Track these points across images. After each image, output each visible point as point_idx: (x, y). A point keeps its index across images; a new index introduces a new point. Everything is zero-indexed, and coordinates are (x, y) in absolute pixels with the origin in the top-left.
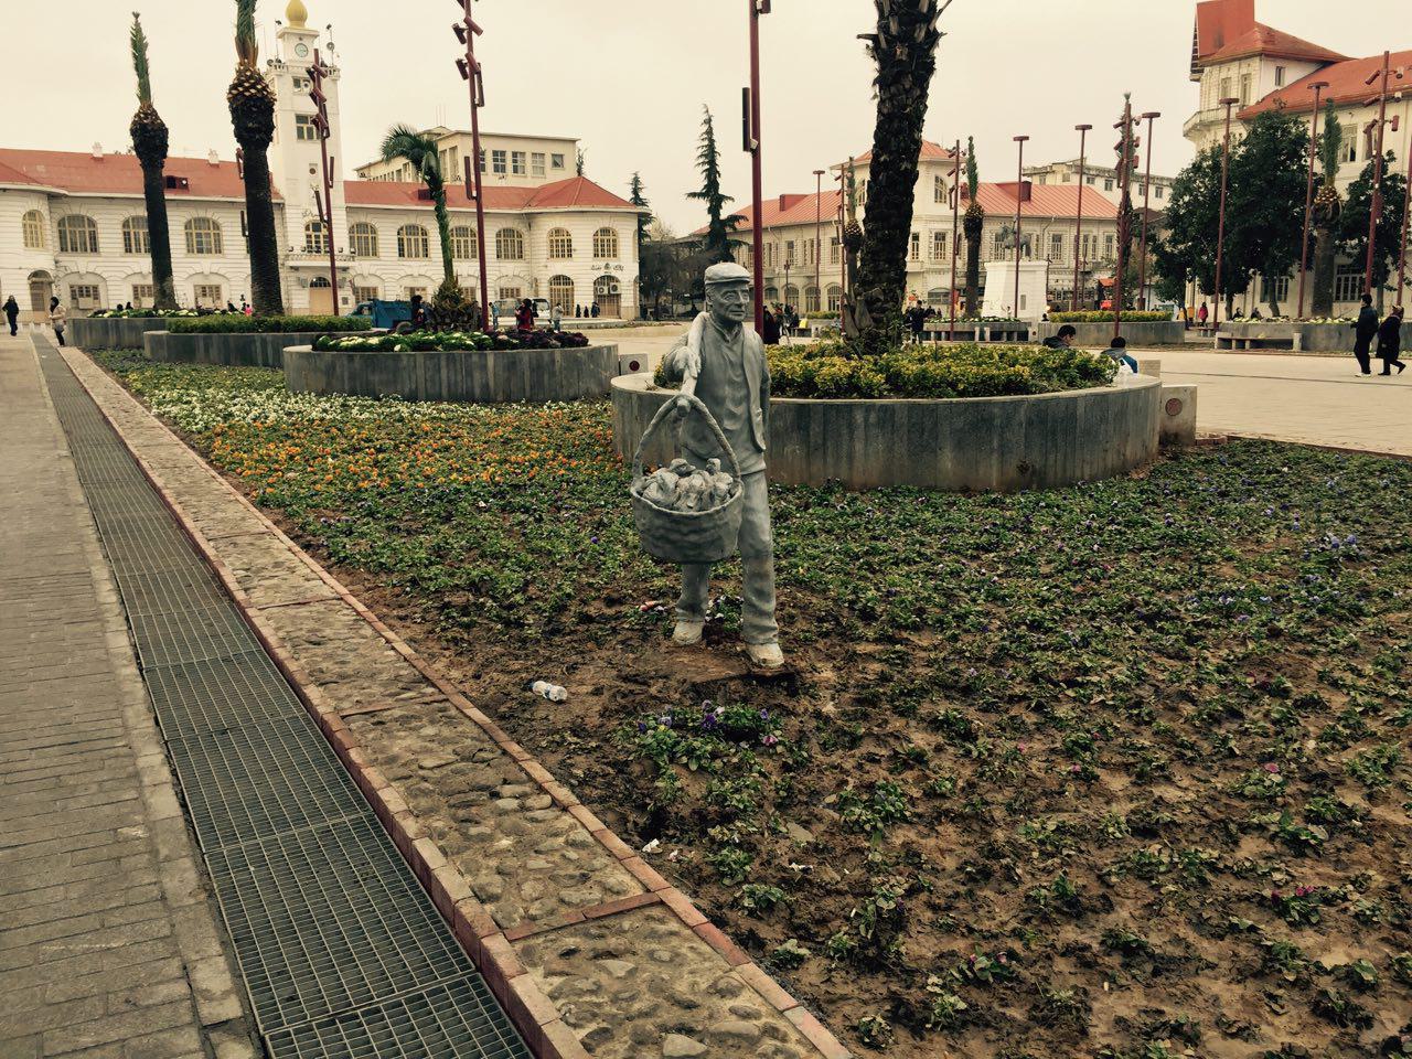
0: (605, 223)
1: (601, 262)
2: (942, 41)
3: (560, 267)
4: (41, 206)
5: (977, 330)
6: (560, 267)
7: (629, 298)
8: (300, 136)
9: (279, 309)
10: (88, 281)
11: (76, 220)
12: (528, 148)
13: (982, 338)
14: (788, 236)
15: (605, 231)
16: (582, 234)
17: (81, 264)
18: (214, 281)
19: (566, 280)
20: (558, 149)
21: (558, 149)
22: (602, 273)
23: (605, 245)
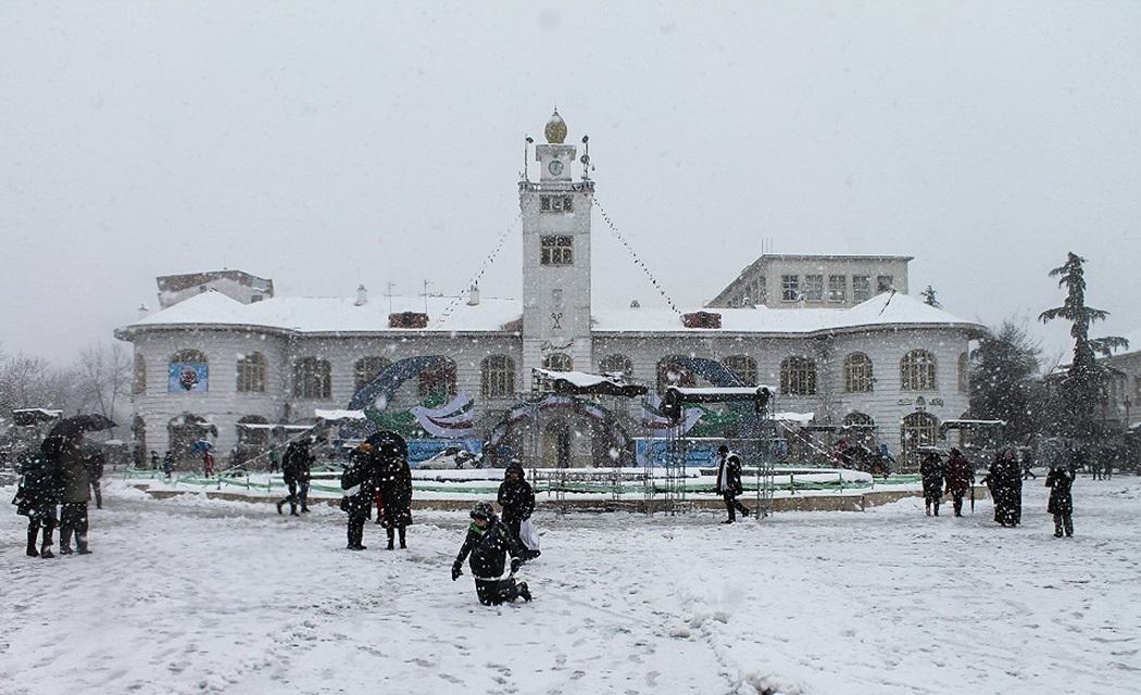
1: (913, 396)
21: (882, 270)
22: (912, 410)
23: (918, 372)
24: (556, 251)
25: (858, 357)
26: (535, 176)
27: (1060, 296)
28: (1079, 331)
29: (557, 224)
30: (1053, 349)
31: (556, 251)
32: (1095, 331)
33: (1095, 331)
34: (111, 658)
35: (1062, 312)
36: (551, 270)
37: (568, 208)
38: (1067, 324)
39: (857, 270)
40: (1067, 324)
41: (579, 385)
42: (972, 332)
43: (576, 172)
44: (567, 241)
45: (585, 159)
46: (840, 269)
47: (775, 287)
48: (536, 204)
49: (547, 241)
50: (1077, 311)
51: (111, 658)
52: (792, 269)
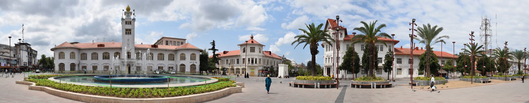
0: (193, 52)
1: (192, 61)
2: (285, 57)
3: (183, 62)
4: (76, 52)
5: (372, 84)
6: (183, 62)
7: (198, 69)
8: (126, 34)
9: (409, 59)
10: (85, 65)
11: (84, 54)
12: (173, 40)
13: (373, 88)
14: (275, 60)
15: (193, 54)
16: (188, 55)
17: (83, 62)
18: (108, 65)
19: (184, 65)
20: (182, 41)
21: (182, 41)
23: (193, 57)
24: (128, 32)
25: (183, 54)
26: (124, 17)
27: (211, 47)
28: (214, 53)
29: (128, 27)
30: (211, 54)
31: (128, 32)
32: (216, 53)
33: (216, 53)
34: (486, 24)
35: (212, 49)
36: (127, 36)
37: (130, 23)
38: (212, 51)
39: (178, 41)
40: (212, 51)
41: (316, 56)
42: (201, 51)
43: (132, 17)
44: (130, 30)
45: (134, 14)
46: (171, 40)
47: (164, 42)
48: (125, 23)
49: (127, 30)
50: (214, 49)
51: (486, 24)
52: (167, 40)
